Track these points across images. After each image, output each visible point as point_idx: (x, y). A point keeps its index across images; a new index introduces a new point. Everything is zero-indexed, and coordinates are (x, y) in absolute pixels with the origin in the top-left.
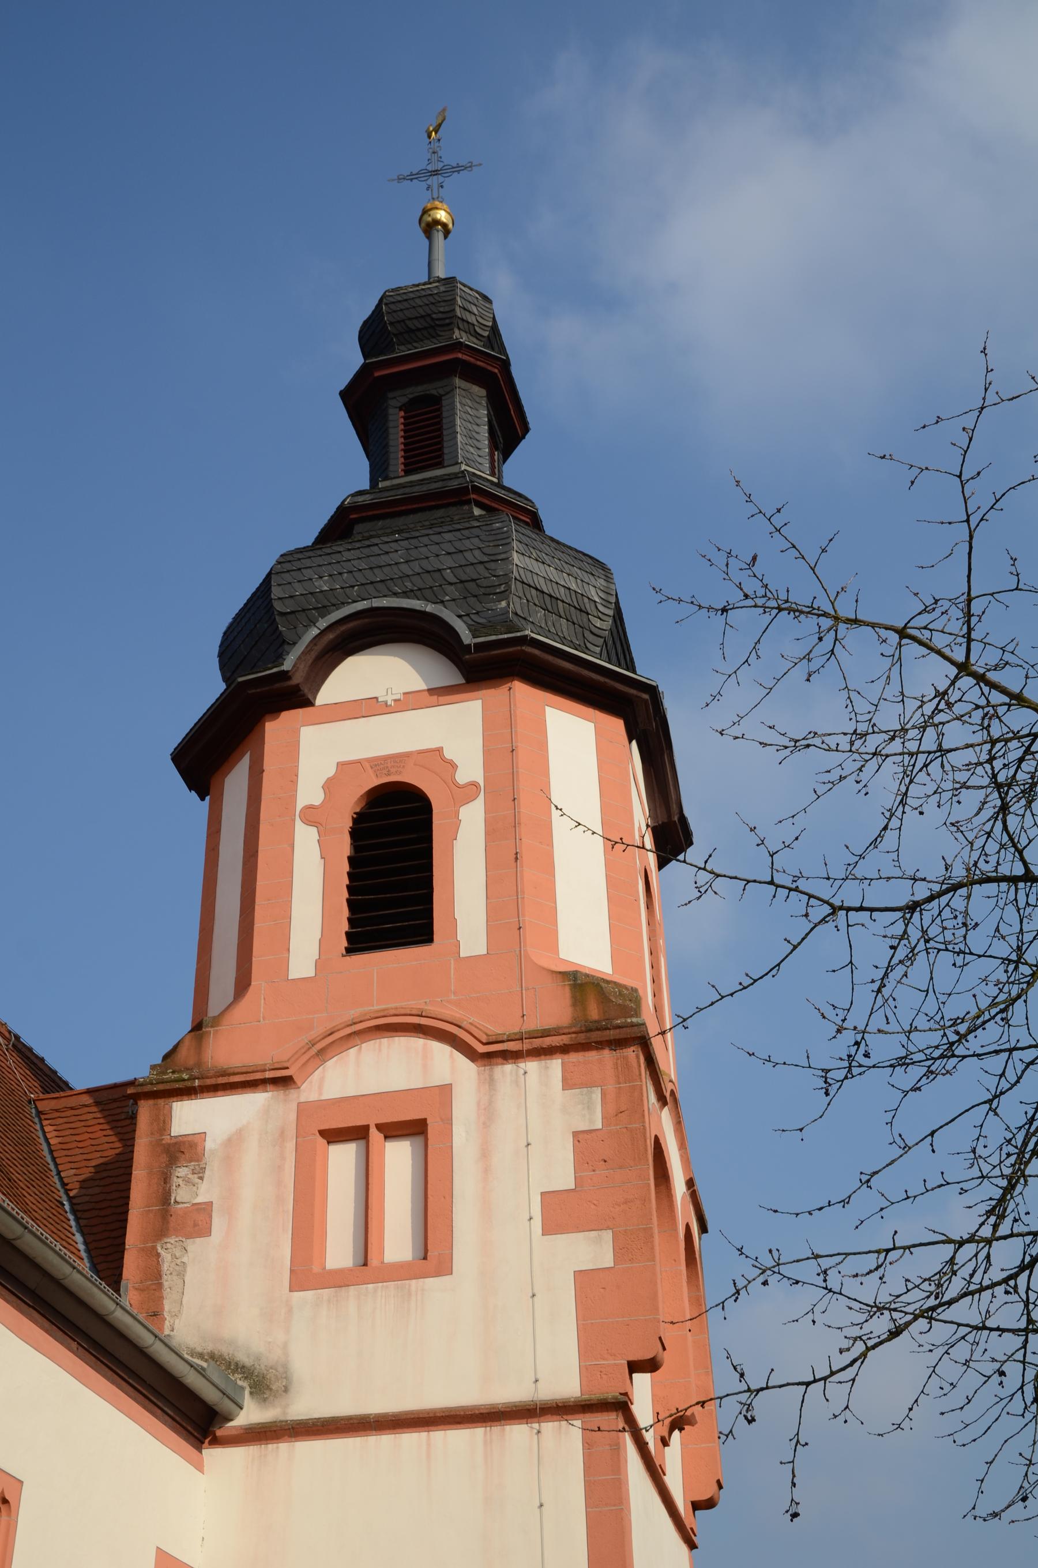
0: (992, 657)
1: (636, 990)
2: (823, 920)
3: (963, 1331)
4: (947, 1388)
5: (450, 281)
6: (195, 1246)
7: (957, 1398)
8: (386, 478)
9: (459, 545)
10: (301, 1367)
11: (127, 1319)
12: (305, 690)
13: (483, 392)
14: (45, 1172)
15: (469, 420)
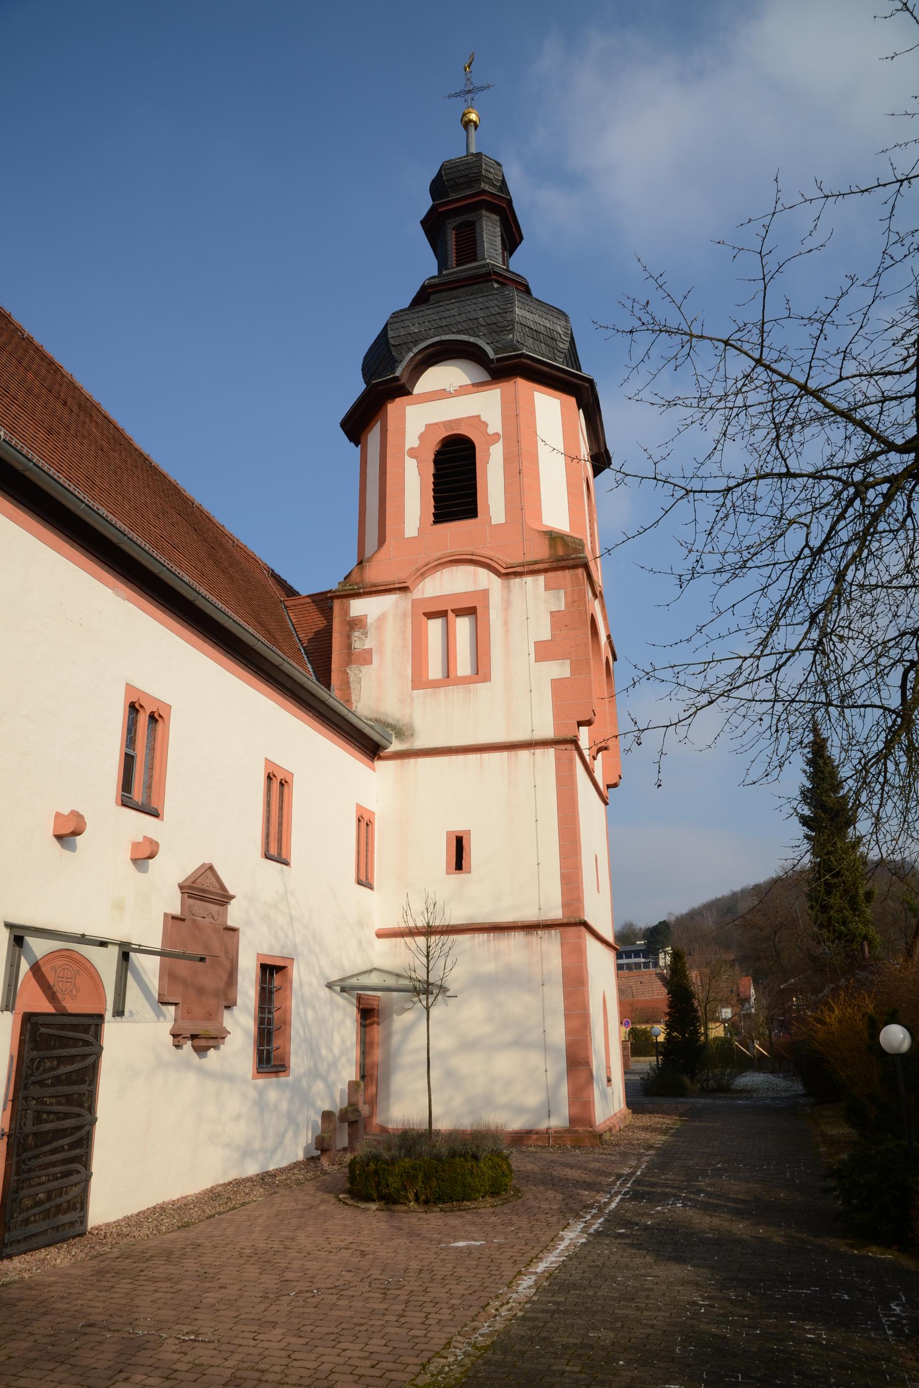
0: (774, 355)
1: (582, 540)
2: (682, 497)
3: (743, 702)
4: (734, 728)
5: (479, 155)
6: (365, 669)
7: (739, 732)
8: (447, 269)
9: (487, 304)
10: (419, 723)
11: (335, 703)
12: (408, 386)
13: (498, 218)
14: (291, 635)
15: (490, 234)
